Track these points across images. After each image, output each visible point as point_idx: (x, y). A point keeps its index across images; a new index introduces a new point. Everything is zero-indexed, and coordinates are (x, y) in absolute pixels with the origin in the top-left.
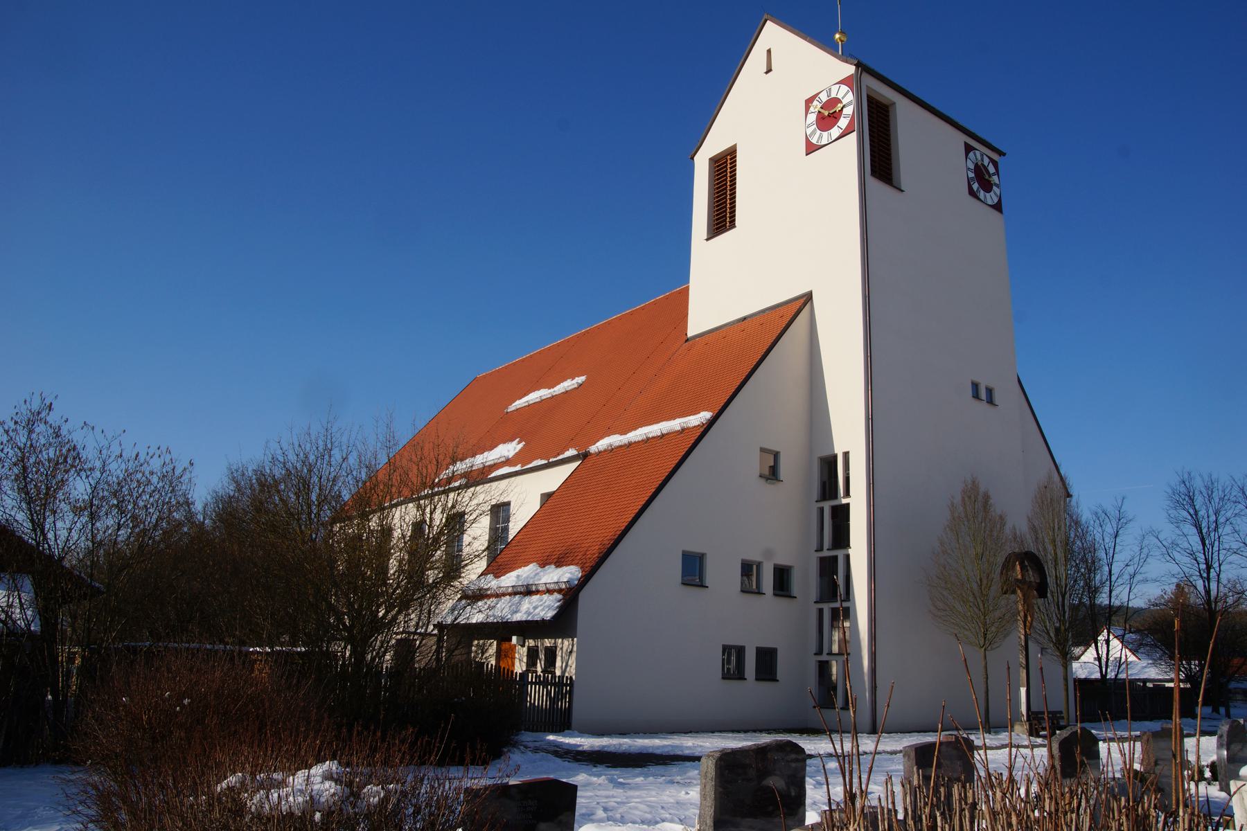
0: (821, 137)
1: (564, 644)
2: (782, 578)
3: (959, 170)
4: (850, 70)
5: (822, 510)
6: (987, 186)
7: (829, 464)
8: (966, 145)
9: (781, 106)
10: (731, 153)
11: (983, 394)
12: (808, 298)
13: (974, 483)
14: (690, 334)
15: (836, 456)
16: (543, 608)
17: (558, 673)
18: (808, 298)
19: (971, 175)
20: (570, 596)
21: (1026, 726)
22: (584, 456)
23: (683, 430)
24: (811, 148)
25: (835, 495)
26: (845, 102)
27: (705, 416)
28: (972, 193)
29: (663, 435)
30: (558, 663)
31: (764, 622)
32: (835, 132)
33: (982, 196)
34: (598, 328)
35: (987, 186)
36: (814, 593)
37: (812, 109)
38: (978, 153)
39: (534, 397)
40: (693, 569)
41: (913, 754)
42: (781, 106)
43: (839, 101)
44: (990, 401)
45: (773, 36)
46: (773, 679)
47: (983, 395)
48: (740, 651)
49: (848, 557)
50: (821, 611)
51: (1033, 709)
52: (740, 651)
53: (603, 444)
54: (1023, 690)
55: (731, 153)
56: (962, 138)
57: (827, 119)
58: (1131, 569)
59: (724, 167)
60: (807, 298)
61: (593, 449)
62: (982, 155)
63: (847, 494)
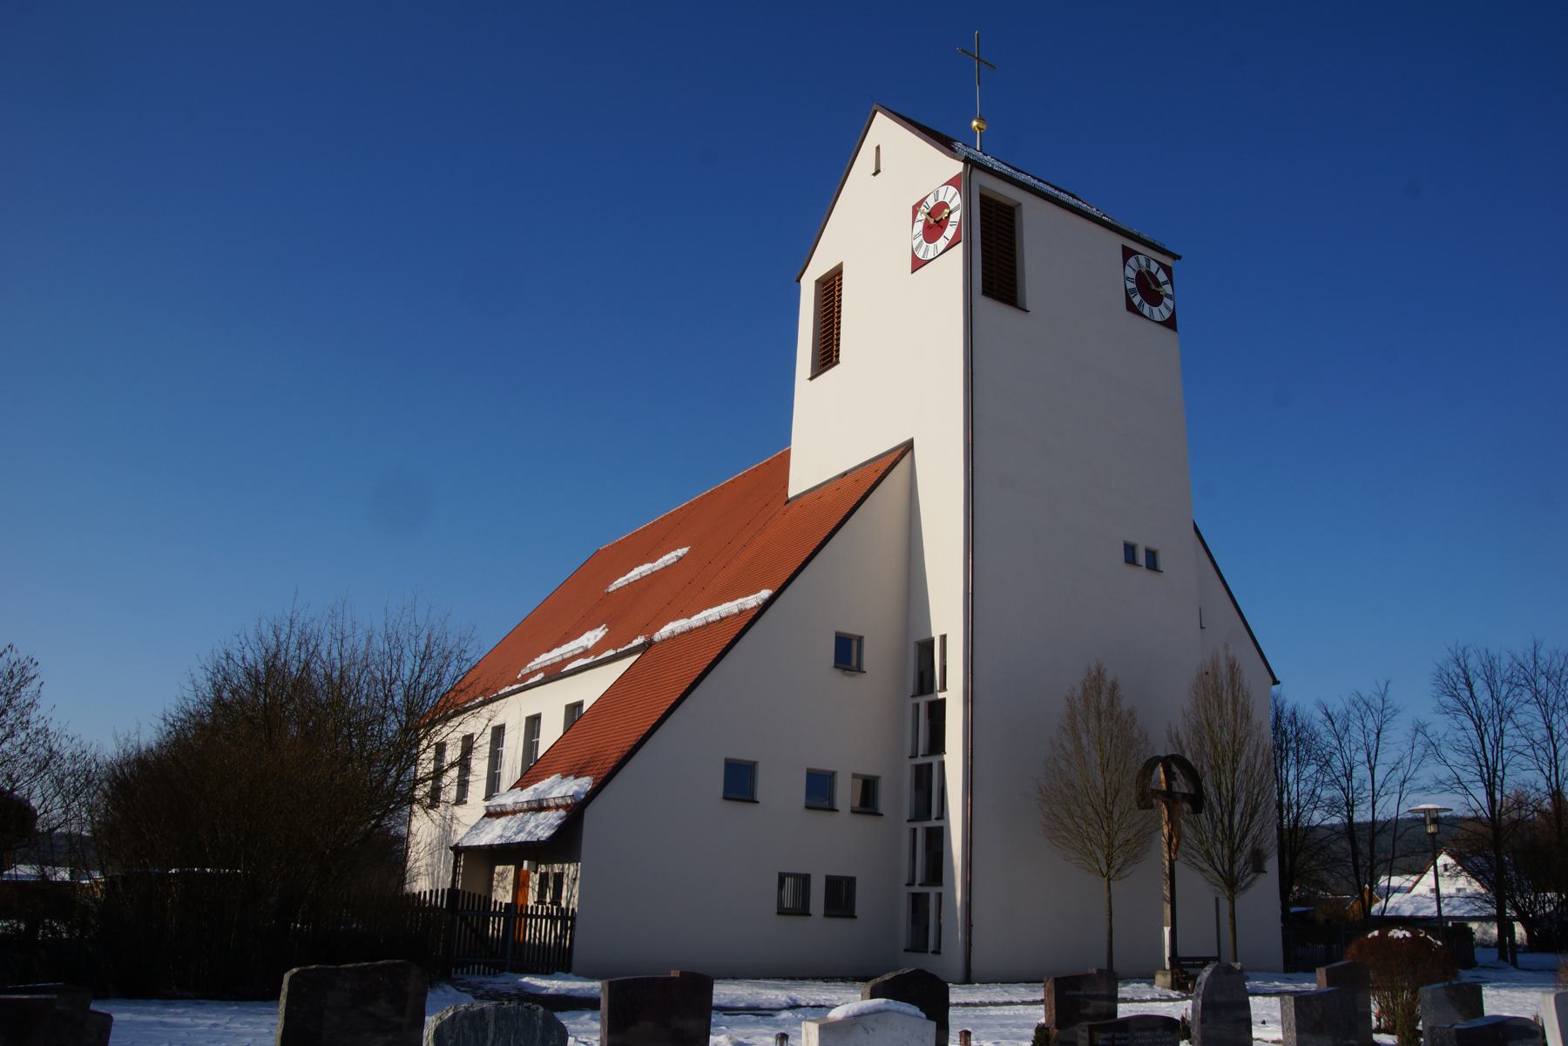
0: (927, 250)
1: (570, 870)
2: (868, 790)
3: (1115, 278)
4: (957, 167)
5: (917, 706)
7: (926, 647)
8: (1125, 249)
12: (908, 447)
13: (1100, 672)
15: (932, 641)
16: (542, 827)
17: (564, 904)
18: (908, 447)
19: (1131, 285)
20: (576, 811)
21: (1169, 978)
23: (741, 612)
24: (917, 264)
25: (931, 690)
26: (952, 206)
27: (765, 594)
28: (1131, 307)
29: (722, 619)
30: (564, 894)
31: (837, 844)
32: (942, 243)
33: (1146, 311)
35: (1155, 299)
36: (907, 809)
38: (1142, 259)
39: (636, 573)
40: (740, 781)
45: (884, 131)
47: (1141, 558)
48: (804, 881)
49: (943, 763)
51: (1180, 954)
52: (804, 881)
53: (665, 631)
54: (1167, 930)
56: (1119, 241)
57: (933, 229)
58: (1400, 774)
59: (830, 287)
61: (657, 637)
62: (1148, 261)
63: (944, 688)
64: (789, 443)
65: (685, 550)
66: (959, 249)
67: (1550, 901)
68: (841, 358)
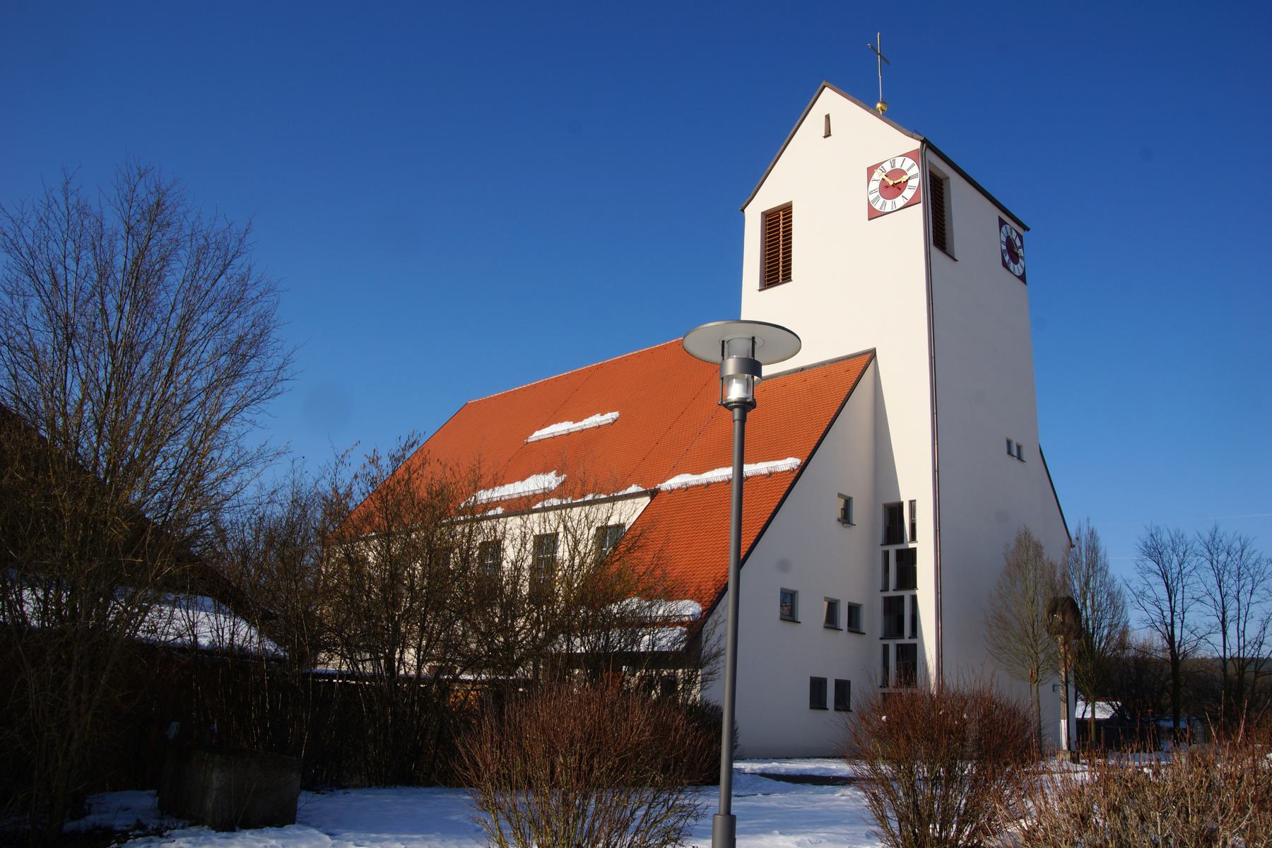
0: (884, 204)
5: (886, 554)
6: (1015, 258)
9: (841, 168)
10: (787, 210)
11: (1015, 451)
12: (872, 354)
15: (901, 505)
22: (654, 494)
23: (771, 474)
24: (873, 214)
25: (901, 539)
28: (1005, 265)
31: (846, 657)
32: (900, 202)
41: (299, 816)
42: (841, 168)
43: (904, 173)
44: (1020, 458)
45: (830, 101)
46: (847, 709)
49: (914, 599)
50: (886, 648)
55: (787, 210)
56: (997, 213)
57: (892, 188)
59: (778, 225)
60: (872, 354)
63: (913, 538)
65: (611, 416)
66: (919, 209)
67: (586, 612)
68: (793, 276)
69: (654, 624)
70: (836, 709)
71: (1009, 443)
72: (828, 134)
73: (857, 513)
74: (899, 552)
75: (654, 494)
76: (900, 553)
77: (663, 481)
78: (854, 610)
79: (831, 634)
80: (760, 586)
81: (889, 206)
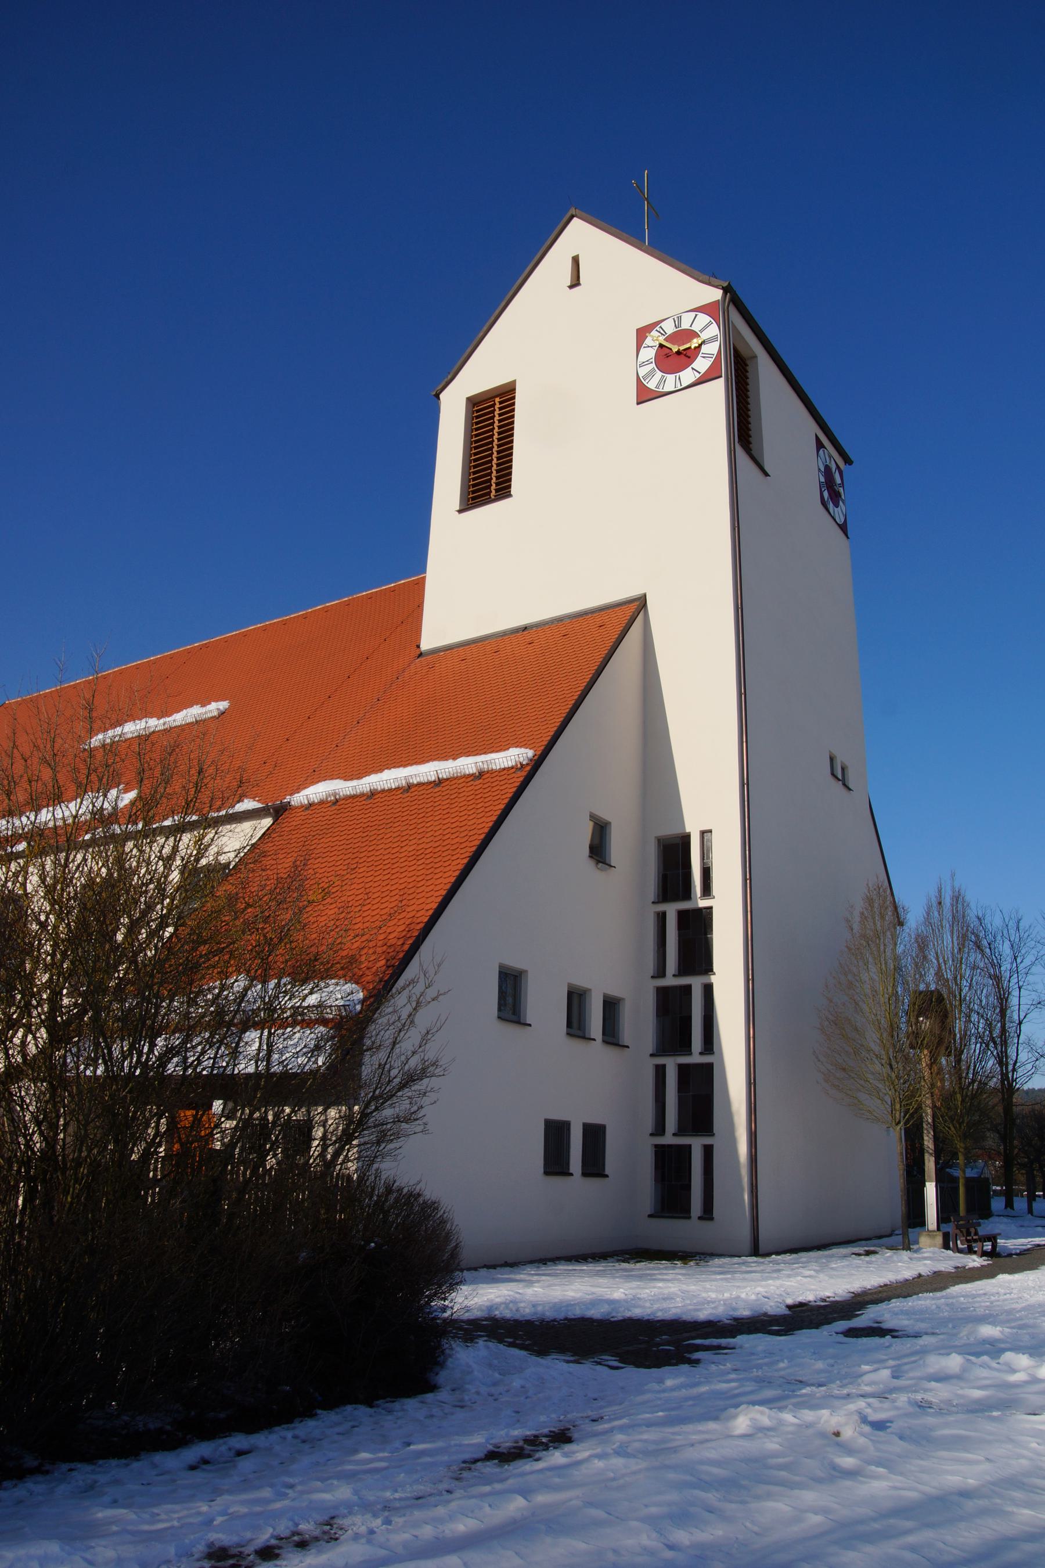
0: (663, 381)
4: (715, 294)
5: (662, 917)
6: (835, 497)
10: (506, 394)
11: (840, 775)
12: (640, 604)
14: (426, 645)
15: (686, 839)
22: (279, 811)
23: (481, 774)
24: (645, 395)
28: (824, 503)
32: (688, 376)
34: (226, 640)
37: (649, 341)
43: (695, 335)
45: (580, 237)
46: (601, 1174)
49: (708, 989)
50: (660, 1072)
55: (506, 394)
57: (675, 356)
59: (493, 420)
60: (640, 604)
63: (707, 890)
64: (423, 569)
68: (513, 490)
69: (270, 1019)
70: (585, 1174)
71: (832, 759)
72: (575, 283)
73: (619, 846)
74: (682, 915)
75: (279, 811)
76: (683, 916)
77: (298, 790)
78: (611, 1005)
79: (577, 1046)
80: (455, 970)
81: (670, 382)
